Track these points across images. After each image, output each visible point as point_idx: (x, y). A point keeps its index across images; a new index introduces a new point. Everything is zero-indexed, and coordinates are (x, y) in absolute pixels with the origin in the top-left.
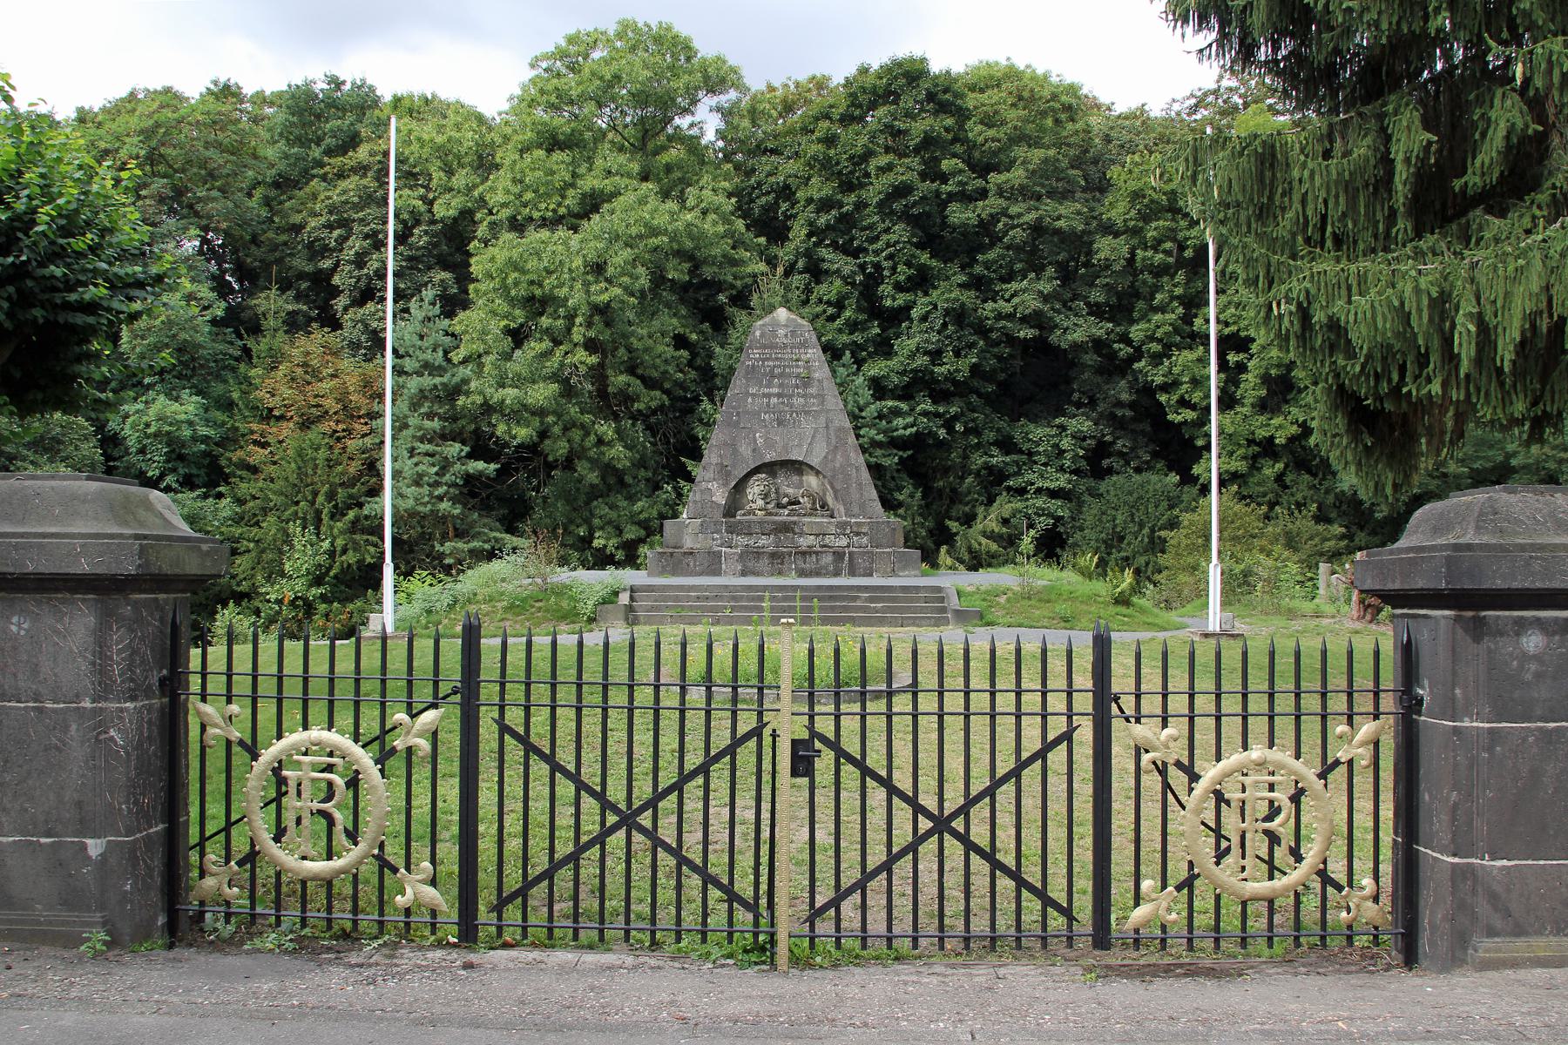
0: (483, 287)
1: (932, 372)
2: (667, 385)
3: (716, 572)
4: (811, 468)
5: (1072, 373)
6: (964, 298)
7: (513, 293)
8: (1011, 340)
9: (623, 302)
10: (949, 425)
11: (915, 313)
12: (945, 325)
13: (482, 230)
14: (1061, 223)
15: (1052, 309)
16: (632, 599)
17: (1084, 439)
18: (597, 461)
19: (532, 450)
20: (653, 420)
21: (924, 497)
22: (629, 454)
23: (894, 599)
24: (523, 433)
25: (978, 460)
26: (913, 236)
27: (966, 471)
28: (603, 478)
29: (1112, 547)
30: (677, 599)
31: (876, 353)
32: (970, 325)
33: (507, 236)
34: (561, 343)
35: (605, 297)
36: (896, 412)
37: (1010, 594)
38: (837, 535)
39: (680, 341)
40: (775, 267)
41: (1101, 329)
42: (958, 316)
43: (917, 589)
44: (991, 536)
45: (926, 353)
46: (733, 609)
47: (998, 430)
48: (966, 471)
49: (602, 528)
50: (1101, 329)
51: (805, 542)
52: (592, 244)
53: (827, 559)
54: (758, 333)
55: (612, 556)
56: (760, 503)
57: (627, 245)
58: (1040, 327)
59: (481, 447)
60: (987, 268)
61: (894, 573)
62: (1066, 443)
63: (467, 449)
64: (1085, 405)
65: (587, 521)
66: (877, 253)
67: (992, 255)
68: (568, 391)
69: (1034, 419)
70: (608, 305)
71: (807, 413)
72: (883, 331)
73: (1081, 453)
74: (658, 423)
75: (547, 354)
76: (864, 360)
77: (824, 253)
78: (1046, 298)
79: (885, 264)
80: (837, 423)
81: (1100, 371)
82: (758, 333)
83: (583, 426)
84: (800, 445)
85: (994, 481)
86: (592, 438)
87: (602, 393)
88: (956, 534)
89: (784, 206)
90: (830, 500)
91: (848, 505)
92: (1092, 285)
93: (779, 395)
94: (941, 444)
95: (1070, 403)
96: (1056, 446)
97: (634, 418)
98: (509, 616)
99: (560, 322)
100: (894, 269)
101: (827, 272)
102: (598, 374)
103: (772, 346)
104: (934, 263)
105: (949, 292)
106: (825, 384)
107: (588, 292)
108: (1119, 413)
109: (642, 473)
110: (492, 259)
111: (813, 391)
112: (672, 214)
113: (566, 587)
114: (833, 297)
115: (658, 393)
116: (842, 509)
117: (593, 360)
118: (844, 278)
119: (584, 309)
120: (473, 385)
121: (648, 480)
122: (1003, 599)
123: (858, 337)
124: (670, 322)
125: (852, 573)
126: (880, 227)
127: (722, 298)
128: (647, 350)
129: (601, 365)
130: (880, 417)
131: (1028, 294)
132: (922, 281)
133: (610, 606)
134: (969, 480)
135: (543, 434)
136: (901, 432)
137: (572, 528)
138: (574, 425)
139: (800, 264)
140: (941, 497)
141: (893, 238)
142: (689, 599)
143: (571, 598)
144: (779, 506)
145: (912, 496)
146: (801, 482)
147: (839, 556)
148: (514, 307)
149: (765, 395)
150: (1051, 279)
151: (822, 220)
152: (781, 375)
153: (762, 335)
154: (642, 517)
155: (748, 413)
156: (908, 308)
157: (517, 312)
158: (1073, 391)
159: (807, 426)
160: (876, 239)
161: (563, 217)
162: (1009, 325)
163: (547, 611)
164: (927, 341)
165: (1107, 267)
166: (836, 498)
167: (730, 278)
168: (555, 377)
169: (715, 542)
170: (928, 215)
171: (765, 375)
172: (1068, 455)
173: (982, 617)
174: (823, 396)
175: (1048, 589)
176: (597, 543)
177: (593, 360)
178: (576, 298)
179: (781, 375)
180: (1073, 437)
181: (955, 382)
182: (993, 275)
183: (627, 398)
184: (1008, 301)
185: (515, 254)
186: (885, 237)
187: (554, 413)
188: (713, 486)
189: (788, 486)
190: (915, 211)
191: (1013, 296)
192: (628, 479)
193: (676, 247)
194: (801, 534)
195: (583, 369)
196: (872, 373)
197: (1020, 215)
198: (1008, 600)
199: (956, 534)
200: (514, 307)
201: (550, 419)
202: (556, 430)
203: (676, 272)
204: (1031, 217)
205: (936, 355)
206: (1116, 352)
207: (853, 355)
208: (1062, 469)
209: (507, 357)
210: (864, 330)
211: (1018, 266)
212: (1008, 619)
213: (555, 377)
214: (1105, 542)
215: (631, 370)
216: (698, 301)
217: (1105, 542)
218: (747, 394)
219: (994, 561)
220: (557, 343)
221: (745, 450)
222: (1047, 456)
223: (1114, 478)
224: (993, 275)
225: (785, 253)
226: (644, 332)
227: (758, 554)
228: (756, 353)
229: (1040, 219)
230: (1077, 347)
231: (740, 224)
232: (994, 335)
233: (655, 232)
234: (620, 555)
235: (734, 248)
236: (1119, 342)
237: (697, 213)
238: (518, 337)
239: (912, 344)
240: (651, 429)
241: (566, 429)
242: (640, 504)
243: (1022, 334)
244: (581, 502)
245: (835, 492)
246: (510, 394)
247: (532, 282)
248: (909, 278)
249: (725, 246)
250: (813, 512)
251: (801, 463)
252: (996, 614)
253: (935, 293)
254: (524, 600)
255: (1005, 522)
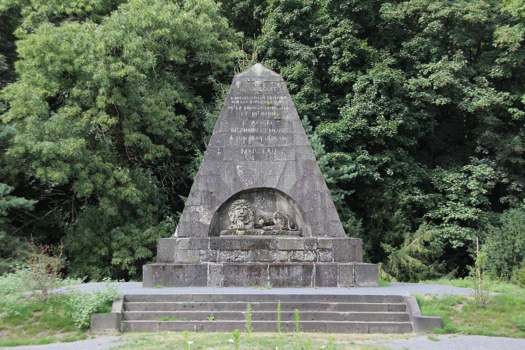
0: (25, 64)
1: (369, 131)
2: (170, 141)
3: (202, 282)
4: (283, 194)
5: (475, 131)
6: (393, 75)
7: (50, 68)
8: (427, 105)
9: (135, 77)
10: (382, 170)
11: (356, 87)
12: (378, 96)
13: (26, 22)
14: (469, 16)
15: (461, 82)
16: (125, 307)
17: (486, 181)
18: (116, 197)
19: (65, 190)
20: (159, 168)
21: (364, 226)
22: (139, 193)
23: (360, 308)
24: (56, 176)
25: (404, 198)
26: (355, 28)
27: (395, 206)
28: (120, 211)
29: (513, 264)
30: (166, 307)
31: (327, 117)
32: (398, 96)
33: (46, 25)
34: (88, 108)
35: (122, 73)
36: (342, 161)
37: (465, 304)
38: (305, 251)
39: (180, 109)
40: (251, 53)
41: (499, 98)
42: (389, 89)
43: (380, 298)
44: (415, 255)
45: (365, 116)
46: (216, 316)
47: (420, 175)
48: (395, 206)
49: (119, 250)
50: (499, 98)
51: (278, 257)
52: (112, 33)
53: (298, 271)
54: (238, 84)
55: (127, 271)
56: (240, 224)
57: (139, 34)
58: (451, 95)
59: (23, 186)
60: (410, 52)
61: (354, 284)
62: (472, 184)
63: (11, 188)
64: (486, 156)
65: (108, 245)
66: (327, 42)
67: (414, 42)
68: (93, 144)
69: (447, 167)
70: (124, 80)
71: (279, 149)
72: (332, 100)
73: (484, 191)
74: (163, 172)
75: (77, 116)
76: (318, 122)
77: (287, 42)
78: (456, 74)
79: (334, 50)
80: (304, 157)
81: (497, 130)
82: (238, 84)
83: (104, 172)
84: (273, 175)
85: (416, 214)
86: (112, 181)
87: (120, 148)
88: (389, 254)
89: (257, 9)
90: (299, 221)
91: (314, 225)
92: (493, 63)
93: (256, 134)
94: (376, 185)
95: (475, 154)
96: (464, 187)
97: (145, 167)
98: (7, 326)
99: (87, 92)
100: (340, 53)
101: (289, 57)
102: (117, 132)
103: (250, 94)
104: (370, 49)
105: (382, 71)
106: (294, 124)
107: (108, 69)
108: (514, 160)
109: (151, 207)
110: (33, 42)
111: (284, 130)
112: (173, 12)
113: (63, 297)
114: (295, 75)
115: (162, 147)
116: (309, 229)
117: (113, 121)
118: (303, 61)
119: (106, 82)
120: (17, 139)
121: (154, 213)
122: (459, 308)
123: (313, 106)
124: (172, 92)
125: (319, 283)
126: (331, 22)
127: (211, 78)
128: (154, 114)
129: (119, 126)
130: (330, 164)
131: (443, 71)
132: (361, 63)
133: (103, 315)
134: (398, 212)
135: (73, 178)
136: (346, 176)
137: (96, 249)
138: (98, 171)
139: (270, 52)
140: (376, 225)
141: (339, 30)
142: (176, 307)
143: (69, 308)
144: (256, 226)
145: (355, 225)
146: (275, 206)
147: (307, 268)
148: (50, 79)
149: (244, 134)
150: (460, 60)
151: (287, 18)
152: (257, 118)
153: (242, 85)
154: (149, 240)
155: (229, 148)
156: (351, 83)
157: (54, 84)
158: (477, 145)
159: (280, 160)
160: (327, 31)
161: (89, 14)
162: (428, 95)
163: (45, 320)
164: (365, 108)
165: (504, 49)
166: (304, 219)
167: (217, 61)
168: (82, 134)
169: (201, 256)
170: (365, 12)
171: (243, 117)
172: (474, 194)
173: (442, 326)
174: (292, 135)
175: (502, 300)
176: (115, 261)
177: (113, 121)
178: (99, 73)
179: (257, 118)
180: (478, 180)
181: (386, 139)
182: (414, 57)
183: (140, 151)
184: (426, 76)
185: (51, 38)
186: (334, 30)
187: (82, 161)
188: (201, 209)
189: (263, 210)
190: (356, 9)
191: (430, 73)
192: (140, 212)
193: (175, 36)
194: (275, 250)
195: (105, 128)
196: (324, 131)
197: (437, 11)
198: (465, 309)
199: (389, 254)
200: (50, 79)
201: (79, 166)
202: (84, 174)
203: (176, 56)
204: (445, 12)
205: (372, 118)
206: (510, 115)
207: (310, 119)
208: (469, 204)
209: (44, 118)
210: (318, 100)
211: (434, 50)
212: (467, 327)
213: (82, 134)
214: (507, 260)
215: (143, 129)
216: (193, 81)
217: (507, 260)
218: (229, 133)
219: (419, 275)
220: (85, 108)
221: (227, 180)
222: (457, 194)
223: (512, 211)
224: (414, 57)
225: (258, 44)
226: (153, 101)
227: (237, 267)
228: (237, 100)
229: (452, 13)
230: (479, 110)
231: (224, 21)
232: (416, 103)
233: (159, 25)
234: (132, 270)
235: (220, 39)
236: (513, 107)
237: (192, 13)
238: (54, 103)
239: (353, 110)
240: (158, 175)
241: (91, 173)
242: (148, 231)
243: (438, 102)
244: (104, 228)
245: (304, 214)
246: (47, 146)
247: (64, 61)
248: (351, 61)
249: (214, 37)
250: (284, 231)
251: (274, 190)
252: (454, 322)
253: (371, 72)
254: (24, 310)
255: (426, 244)
